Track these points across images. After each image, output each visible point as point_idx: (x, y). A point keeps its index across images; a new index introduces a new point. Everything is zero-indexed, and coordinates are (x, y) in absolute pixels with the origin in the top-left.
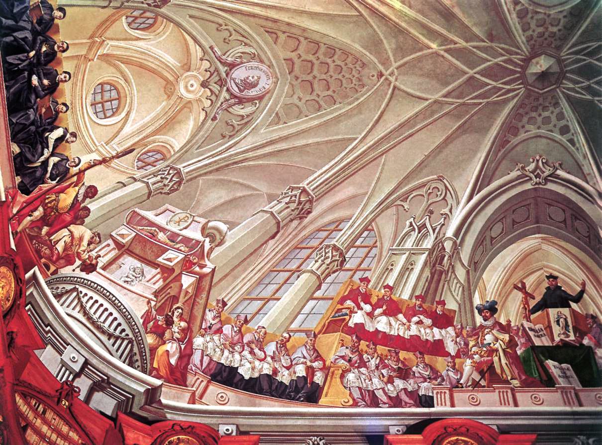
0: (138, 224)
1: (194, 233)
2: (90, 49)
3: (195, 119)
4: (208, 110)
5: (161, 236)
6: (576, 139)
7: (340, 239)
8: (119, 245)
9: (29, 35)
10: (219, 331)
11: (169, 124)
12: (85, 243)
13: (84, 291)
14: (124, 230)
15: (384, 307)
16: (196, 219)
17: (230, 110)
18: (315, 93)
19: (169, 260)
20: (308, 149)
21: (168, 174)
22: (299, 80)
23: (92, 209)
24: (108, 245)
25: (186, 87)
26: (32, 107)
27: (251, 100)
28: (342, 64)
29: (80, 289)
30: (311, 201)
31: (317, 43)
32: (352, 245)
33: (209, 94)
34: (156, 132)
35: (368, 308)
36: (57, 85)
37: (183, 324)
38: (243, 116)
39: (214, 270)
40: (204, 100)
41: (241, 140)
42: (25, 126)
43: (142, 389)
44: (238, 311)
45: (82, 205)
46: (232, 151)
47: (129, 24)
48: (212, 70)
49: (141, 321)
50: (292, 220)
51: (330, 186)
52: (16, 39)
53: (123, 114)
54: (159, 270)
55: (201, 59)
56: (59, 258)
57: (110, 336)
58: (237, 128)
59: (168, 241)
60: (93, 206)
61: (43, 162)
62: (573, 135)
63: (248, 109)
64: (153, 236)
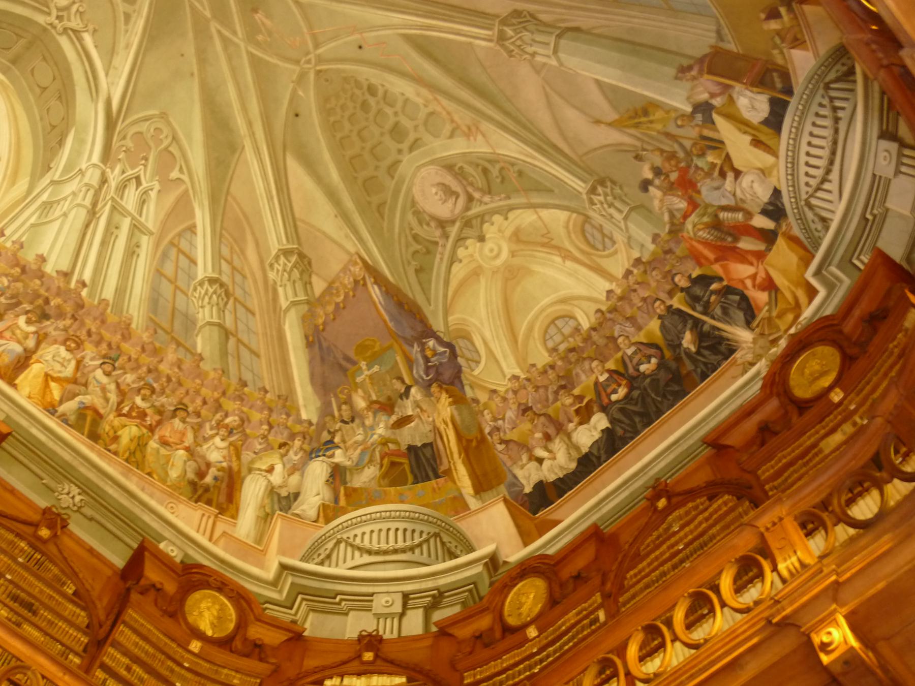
6: (133, 19)
25: (497, 256)
47: (478, 362)
57: (837, 120)
62: (134, 11)
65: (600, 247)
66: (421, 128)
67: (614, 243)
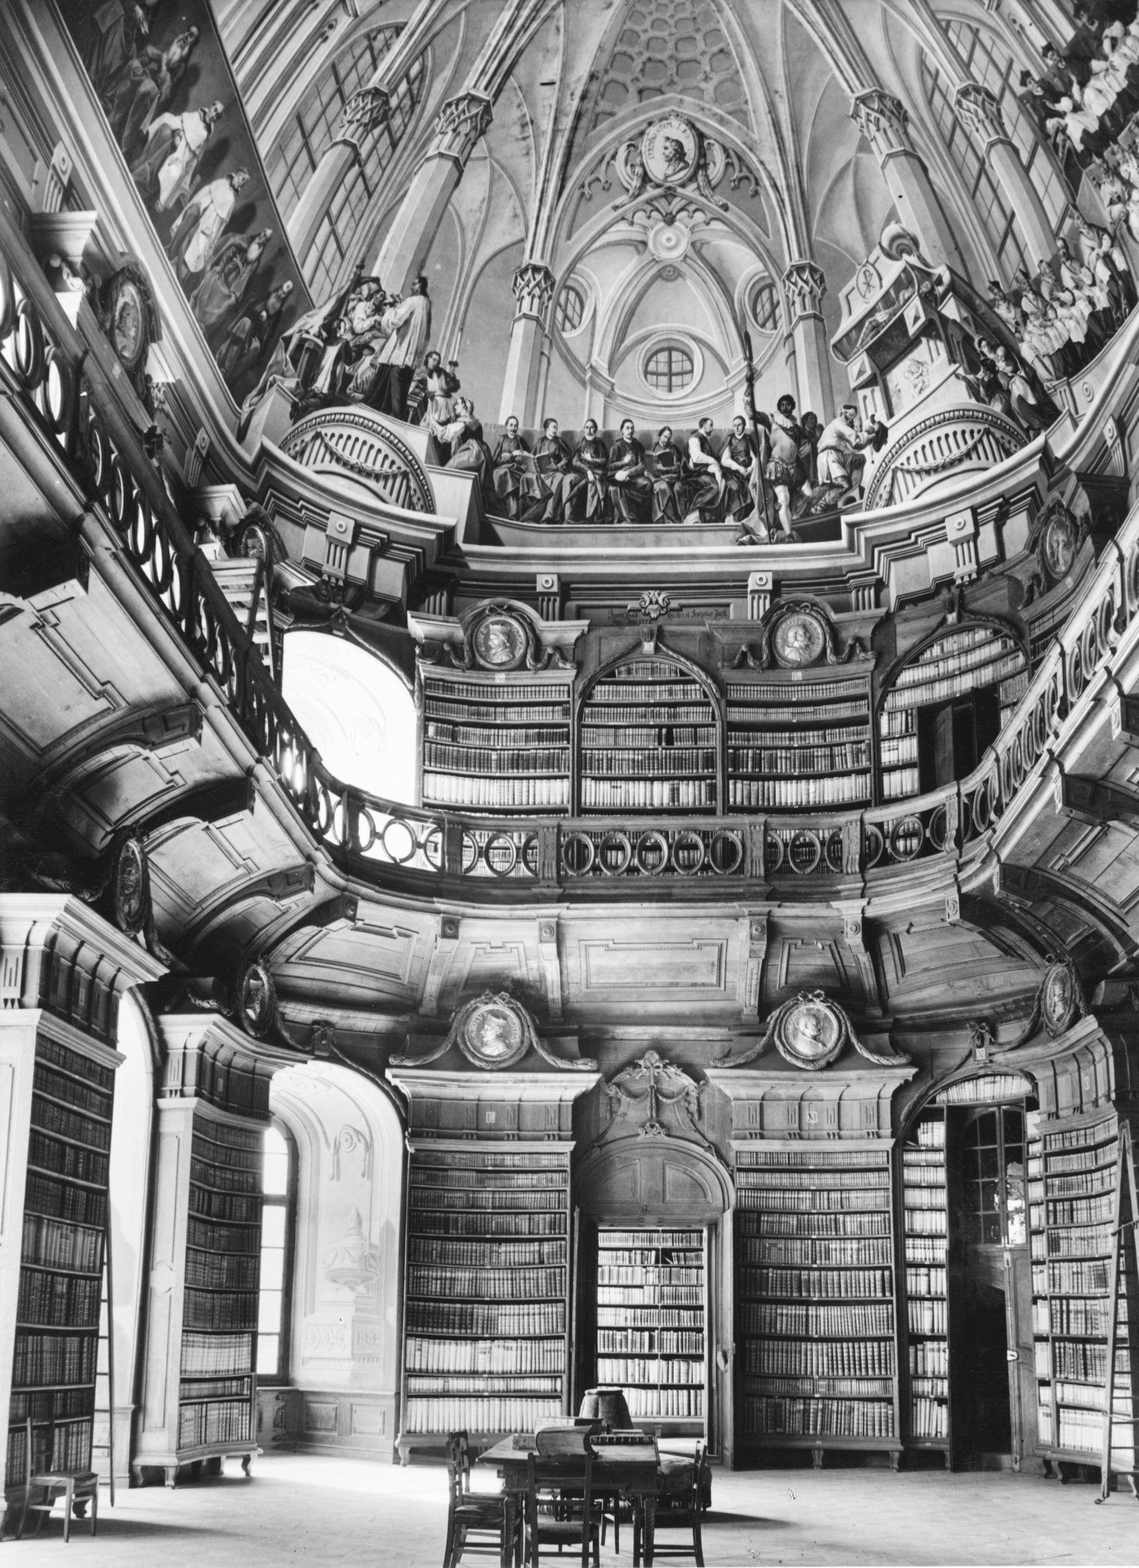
0: (852, 344)
1: (892, 270)
2: (597, 387)
3: (722, 238)
4: (710, 216)
5: (881, 317)
7: (952, 81)
8: (871, 382)
9: (571, 477)
10: (1025, 316)
11: (722, 280)
12: (848, 432)
13: (902, 459)
14: (854, 368)
15: (1074, 78)
16: (872, 259)
17: (713, 183)
18: (699, 58)
19: (916, 319)
20: (794, 78)
21: (795, 284)
22: (676, 79)
23: (809, 410)
24: (865, 398)
25: (670, 249)
26: (652, 484)
27: (702, 152)
28: (649, 20)
29: (897, 464)
30: (882, 97)
31: (614, 57)
32: (966, 66)
33: (683, 214)
34: (728, 294)
35: (1065, 104)
36: (633, 440)
37: (1000, 351)
38: (728, 165)
39: (950, 269)
40: (692, 222)
41: (766, 169)
42: (672, 499)
43: (1035, 467)
44: (1011, 276)
45: (799, 423)
46: (781, 183)
47: (574, 327)
48: (649, 208)
49: (973, 401)
50: (906, 133)
51: (860, 57)
52: (570, 500)
53: (694, 346)
54: (924, 340)
55: (632, 223)
56: (847, 478)
57: (968, 455)
58: (745, 173)
59: (890, 310)
60: (806, 404)
61: (724, 476)
63: (717, 156)
64: (876, 327)
65: (761, 319)
66: (707, 57)
67: (775, 327)
